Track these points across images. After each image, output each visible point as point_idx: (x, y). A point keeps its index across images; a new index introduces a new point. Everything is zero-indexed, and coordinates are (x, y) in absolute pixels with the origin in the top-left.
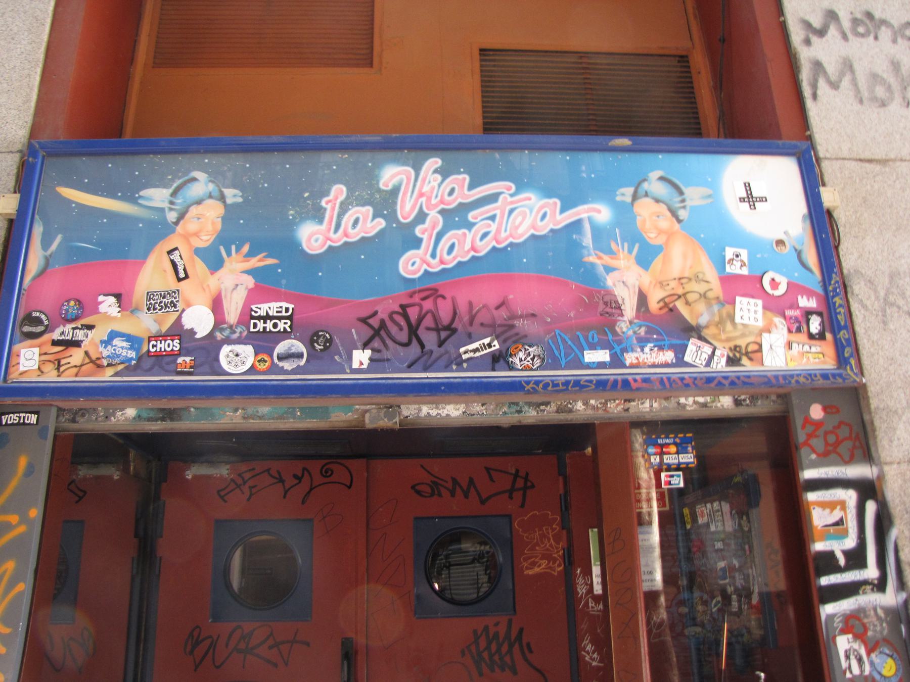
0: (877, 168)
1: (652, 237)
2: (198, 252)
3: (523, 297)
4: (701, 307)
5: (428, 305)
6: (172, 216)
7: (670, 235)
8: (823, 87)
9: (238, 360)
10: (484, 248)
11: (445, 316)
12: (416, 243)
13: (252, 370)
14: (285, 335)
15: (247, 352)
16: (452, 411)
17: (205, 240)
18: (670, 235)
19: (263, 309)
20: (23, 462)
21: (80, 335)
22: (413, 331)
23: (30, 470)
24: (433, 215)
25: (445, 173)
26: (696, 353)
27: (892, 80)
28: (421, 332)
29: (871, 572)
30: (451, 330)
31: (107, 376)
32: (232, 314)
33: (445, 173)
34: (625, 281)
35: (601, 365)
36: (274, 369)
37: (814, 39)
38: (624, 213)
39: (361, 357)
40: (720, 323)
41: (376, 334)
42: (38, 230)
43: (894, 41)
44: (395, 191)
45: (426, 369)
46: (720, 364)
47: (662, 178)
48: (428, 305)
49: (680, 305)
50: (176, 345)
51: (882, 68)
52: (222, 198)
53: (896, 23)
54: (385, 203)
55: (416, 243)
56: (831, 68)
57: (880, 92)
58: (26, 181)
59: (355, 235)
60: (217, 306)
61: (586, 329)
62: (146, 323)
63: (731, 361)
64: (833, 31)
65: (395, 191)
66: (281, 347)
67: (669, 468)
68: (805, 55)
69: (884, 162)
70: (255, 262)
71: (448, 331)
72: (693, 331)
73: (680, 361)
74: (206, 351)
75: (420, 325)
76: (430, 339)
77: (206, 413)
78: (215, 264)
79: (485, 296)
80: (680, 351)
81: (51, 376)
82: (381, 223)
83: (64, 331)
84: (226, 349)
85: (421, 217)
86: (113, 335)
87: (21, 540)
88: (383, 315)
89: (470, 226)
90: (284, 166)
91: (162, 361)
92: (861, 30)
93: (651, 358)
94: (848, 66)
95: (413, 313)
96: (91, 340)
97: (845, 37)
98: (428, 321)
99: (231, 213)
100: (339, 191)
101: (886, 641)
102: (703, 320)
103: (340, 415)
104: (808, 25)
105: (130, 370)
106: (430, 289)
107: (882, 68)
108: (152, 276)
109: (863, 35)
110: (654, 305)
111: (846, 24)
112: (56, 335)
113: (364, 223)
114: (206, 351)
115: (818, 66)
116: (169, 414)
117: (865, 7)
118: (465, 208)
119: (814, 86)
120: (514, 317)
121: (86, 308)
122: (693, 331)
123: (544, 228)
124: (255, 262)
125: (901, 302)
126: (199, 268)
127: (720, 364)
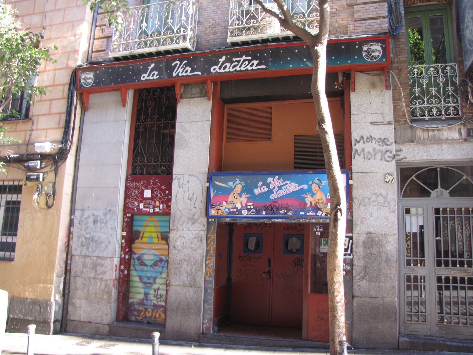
0: (365, 174)
1: (314, 191)
2: (238, 194)
3: (290, 203)
4: (321, 205)
5: (275, 204)
6: (233, 187)
7: (317, 191)
8: (356, 155)
9: (245, 213)
10: (285, 193)
11: (277, 206)
12: (273, 193)
13: (247, 214)
14: (252, 209)
15: (246, 211)
16: (280, 220)
17: (239, 192)
18: (317, 191)
19: (248, 204)
20: (213, 227)
21: (220, 208)
22: (272, 208)
23: (214, 228)
24: (276, 187)
25: (278, 179)
26: (319, 213)
27: (373, 153)
28: (274, 209)
29: (349, 252)
30: (278, 208)
31: (225, 215)
32: (244, 205)
33: (278, 179)
34: (309, 200)
35: (302, 215)
36: (251, 214)
37: (357, 144)
38: (310, 187)
39: (264, 213)
40: (325, 208)
41: (266, 209)
42: (212, 190)
43: (375, 143)
44: (270, 182)
45: (274, 215)
46: (323, 215)
47: (318, 179)
48: (275, 204)
49: (318, 204)
50: (235, 210)
51: (371, 150)
52: (241, 184)
53: (376, 138)
54: (268, 185)
55: (273, 193)
56: (359, 151)
57: (369, 156)
58: (209, 180)
59: (263, 191)
60: (241, 203)
61: (300, 209)
62: (230, 206)
63: (326, 215)
64: (362, 141)
65: (270, 182)
66: (251, 211)
67: (318, 231)
68: (354, 148)
69: (366, 173)
70: (247, 196)
71: (278, 209)
72: (320, 209)
73: (316, 215)
74: (240, 211)
75: (272, 208)
76: (275, 210)
77: (240, 220)
78: (241, 196)
79: (284, 202)
80: (317, 213)
81: (216, 214)
82: (267, 189)
83: (218, 207)
84: (243, 211)
85: (274, 188)
86: (226, 208)
87: (213, 239)
88: (267, 206)
89: (282, 190)
90: (251, 178)
91: (233, 213)
92: (368, 140)
93: (312, 214)
94: (363, 150)
95: (272, 205)
96: (222, 209)
97: (364, 143)
98: (275, 207)
99: (243, 187)
100: (261, 183)
101: (349, 264)
102: (322, 207)
103: (262, 221)
104: (356, 140)
105: (228, 214)
106: (275, 201)
107: (371, 150)
108: (231, 198)
109: (368, 142)
110: (313, 204)
111: (365, 139)
112: (217, 208)
113: (265, 189)
114: (240, 211)
115: (356, 150)
116: (235, 220)
117: (370, 134)
118: (282, 186)
119: (355, 156)
120: (288, 206)
121: (221, 203)
122: (320, 209)
123: (295, 190)
124: (247, 196)
125: (363, 203)
126: (238, 197)
127: (323, 215)
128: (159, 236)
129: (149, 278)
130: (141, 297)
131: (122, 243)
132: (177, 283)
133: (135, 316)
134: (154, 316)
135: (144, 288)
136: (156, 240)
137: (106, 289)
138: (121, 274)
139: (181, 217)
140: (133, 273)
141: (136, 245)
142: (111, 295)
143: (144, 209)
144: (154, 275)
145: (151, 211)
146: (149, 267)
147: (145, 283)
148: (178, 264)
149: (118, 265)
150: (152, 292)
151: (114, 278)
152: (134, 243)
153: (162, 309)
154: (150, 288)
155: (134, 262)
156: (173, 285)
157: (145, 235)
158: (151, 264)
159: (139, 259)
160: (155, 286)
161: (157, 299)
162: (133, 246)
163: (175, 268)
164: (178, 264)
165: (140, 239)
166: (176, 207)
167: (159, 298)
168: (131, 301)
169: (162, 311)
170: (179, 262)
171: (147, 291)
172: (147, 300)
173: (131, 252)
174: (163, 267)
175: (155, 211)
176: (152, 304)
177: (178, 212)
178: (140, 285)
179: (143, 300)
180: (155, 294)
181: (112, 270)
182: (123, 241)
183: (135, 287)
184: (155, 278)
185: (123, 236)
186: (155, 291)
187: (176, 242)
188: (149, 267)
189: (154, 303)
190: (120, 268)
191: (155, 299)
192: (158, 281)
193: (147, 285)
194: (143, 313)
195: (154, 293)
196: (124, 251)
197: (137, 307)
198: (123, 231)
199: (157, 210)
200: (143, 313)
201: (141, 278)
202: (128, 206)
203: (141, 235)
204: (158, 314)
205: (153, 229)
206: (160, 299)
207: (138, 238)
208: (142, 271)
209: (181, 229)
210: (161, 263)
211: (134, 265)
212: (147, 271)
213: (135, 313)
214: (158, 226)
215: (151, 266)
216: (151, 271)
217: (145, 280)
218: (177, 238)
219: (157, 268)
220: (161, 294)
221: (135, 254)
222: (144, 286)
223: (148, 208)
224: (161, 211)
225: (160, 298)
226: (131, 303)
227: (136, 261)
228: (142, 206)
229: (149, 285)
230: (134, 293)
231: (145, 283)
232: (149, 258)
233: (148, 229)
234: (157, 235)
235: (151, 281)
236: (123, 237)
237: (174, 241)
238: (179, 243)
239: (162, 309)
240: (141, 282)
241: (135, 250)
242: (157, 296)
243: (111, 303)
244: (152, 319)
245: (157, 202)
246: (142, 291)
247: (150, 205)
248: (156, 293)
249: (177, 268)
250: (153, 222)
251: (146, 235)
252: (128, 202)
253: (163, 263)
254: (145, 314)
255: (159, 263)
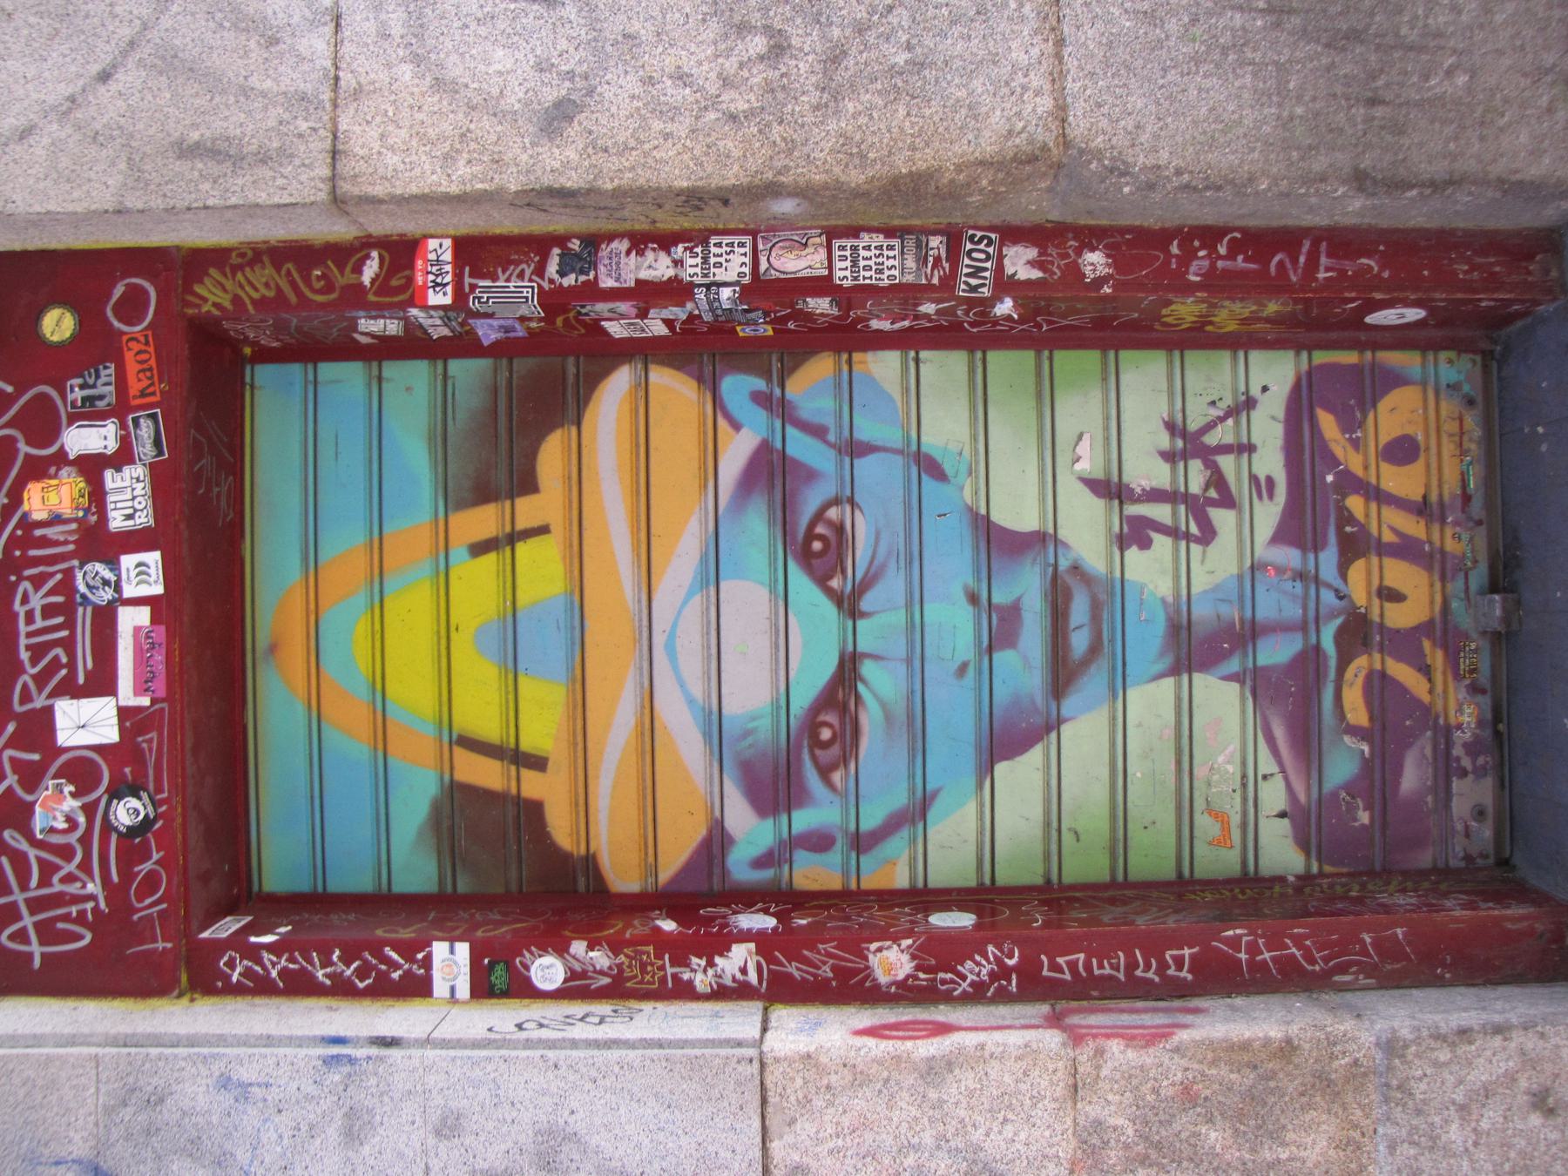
128: (484, 521)
129: (1001, 628)
130: (1220, 700)
131: (577, 988)
132: (1024, 48)
133: (1445, 769)
134: (1414, 527)
135: (1118, 685)
136: (542, 568)
137: (1214, 1137)
138: (975, 969)
139: (170, 64)
140: (950, 849)
141: (617, 838)
142: (1287, 1049)
143: (127, 693)
144: (952, 562)
145: (143, 574)
146: (868, 635)
147: (1062, 674)
148: (779, 49)
149: (866, 1017)
150: (1151, 571)
151: (1052, 1039)
152: (590, 862)
153: (1328, 423)
154: (1109, 596)
155: (819, 842)
156: (1061, 112)
157: (490, 728)
158: (828, 608)
159: (774, 787)
160: (1086, 530)
161: (1227, 501)
162: (624, 878)
163: (831, 95)
164: (779, 49)
165: (532, 785)
166: (39, 146)
167: (1217, 479)
168: (1281, 852)
169: (1349, 424)
170: (758, 44)
171: (1145, 639)
172: (1249, 633)
173: (698, 903)
174: (855, 449)
175: (144, 519)
176: (1290, 556)
177: (107, 105)
178: (1084, 734)
179: (1258, 684)
180: (1173, 532)
181: (933, 1071)
182: (547, 971)
183: (1119, 813)
184: (996, 543)
185: (482, 989)
186: (1136, 534)
187: (491, 106)
188: (868, 635)
189: (1278, 538)
190: (906, 993)
191: (1223, 518)
192: (1017, 510)
193: (1079, 642)
194: (1402, 672)
195: (1161, 543)
196: (680, 951)
197: (1343, 763)
198: (418, 987)
199: (129, 498)
200: (1402, 672)
201: (1003, 740)
202: (98, 923)
203: (487, 774)
204: (1402, 481)
205: (411, 607)
206: (1226, 463)
207: (533, 811)
208: (914, 726)
209: (317, 44)
210: (811, 475)
211: (861, 843)
212: (916, 660)
213: (1412, 777)
214: (377, 545)
215: (850, 606)
216: (916, 599)
217: (1022, 670)
218: (439, 84)
219: (863, 532)
220: (1169, 456)
221: (717, 841)
222: (1093, 683)
223: (105, 619)
224: (144, 446)
225: (1209, 455)
226: (1303, 843)
227: (803, 820)
228: (86, 723)
229: (1079, 612)
230: (1185, 809)
231: (1062, 674)
232: (751, 647)
233: (413, 692)
234: (480, 549)
235: (1025, 586)
236: (497, 980)
237: (485, 127)
238: (501, 59)
239: (1328, 423)
240: (1053, 725)
241: (676, 852)
242: (1199, 509)
243: (1392, 1047)
244: (1453, 541)
245: (41, 500)
246: (1151, 702)
247: (67, 605)
248: (1161, 512)
249: (835, 57)
250: (333, 620)
251: (480, 713)
252: (47, 932)
253: (800, 446)
254: (1404, 644)
255: (811, 500)
